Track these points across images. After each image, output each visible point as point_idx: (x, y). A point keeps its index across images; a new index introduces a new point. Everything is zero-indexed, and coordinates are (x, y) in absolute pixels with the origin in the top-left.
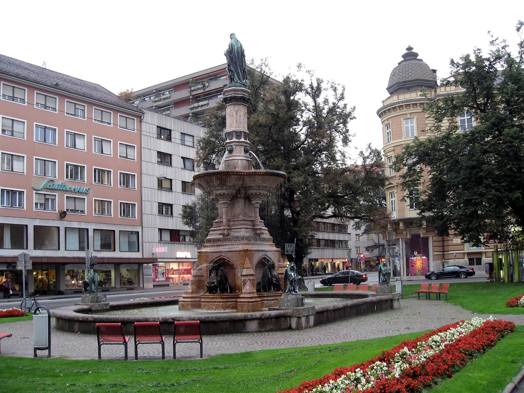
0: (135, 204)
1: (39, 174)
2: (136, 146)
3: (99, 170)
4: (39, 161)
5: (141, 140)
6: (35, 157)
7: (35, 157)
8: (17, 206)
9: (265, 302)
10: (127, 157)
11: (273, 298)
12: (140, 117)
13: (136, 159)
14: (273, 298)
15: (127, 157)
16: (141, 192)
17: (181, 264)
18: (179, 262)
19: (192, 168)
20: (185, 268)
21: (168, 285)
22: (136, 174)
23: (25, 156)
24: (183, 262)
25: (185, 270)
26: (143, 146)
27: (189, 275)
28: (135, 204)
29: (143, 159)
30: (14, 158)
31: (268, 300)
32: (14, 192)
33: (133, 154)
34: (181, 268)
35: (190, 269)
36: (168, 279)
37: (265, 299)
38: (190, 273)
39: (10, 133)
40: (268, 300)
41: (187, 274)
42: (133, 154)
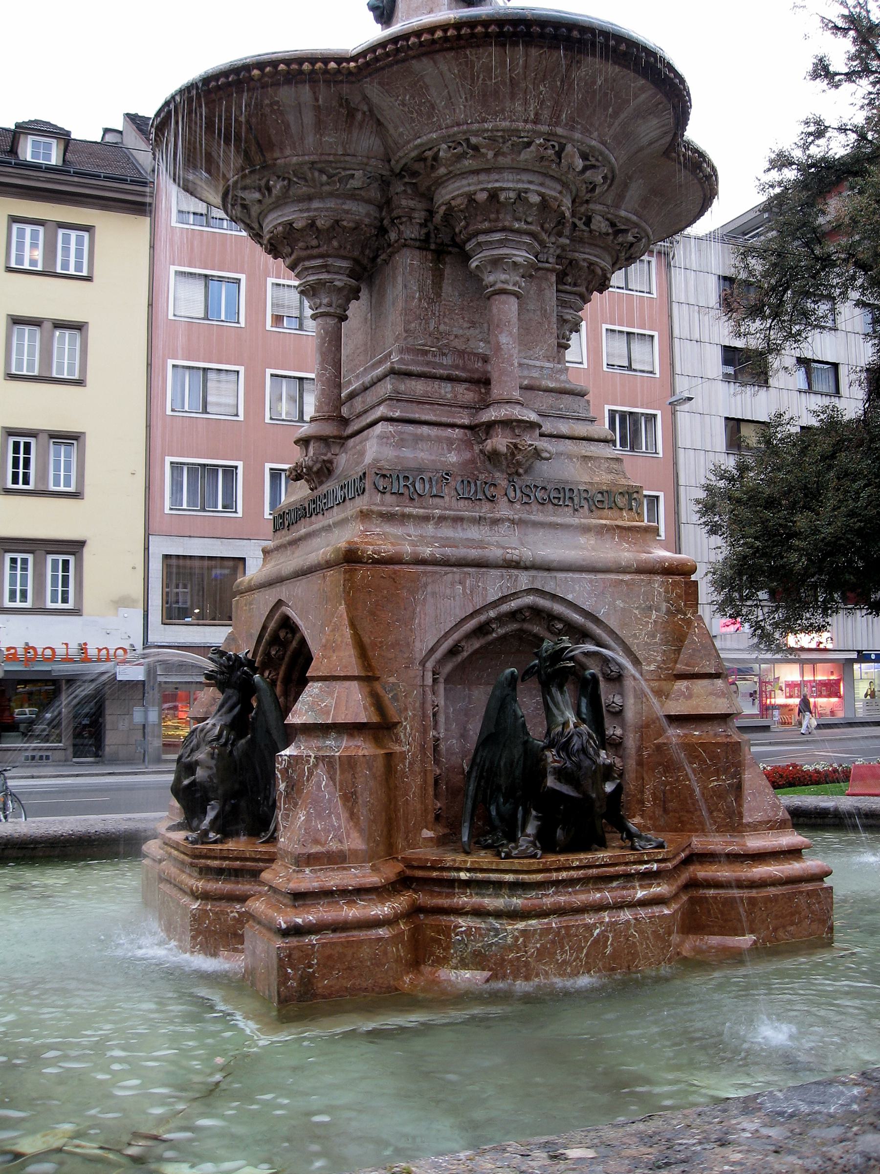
0: (657, 497)
1: (186, 408)
2: (655, 334)
3: (623, 415)
4: (284, 381)
5: (671, 316)
6: (269, 371)
7: (269, 371)
8: (220, 508)
9: (463, 923)
10: (630, 368)
11: (517, 902)
12: (667, 254)
13: (657, 371)
14: (517, 902)
15: (630, 368)
16: (675, 464)
17: (808, 668)
18: (802, 662)
19: (832, 389)
20: (820, 677)
21: (766, 728)
22: (658, 413)
23: (241, 369)
24: (813, 662)
25: (822, 684)
26: (676, 333)
27: (834, 700)
28: (657, 497)
29: (678, 370)
30: (211, 376)
31: (479, 913)
32: (213, 470)
33: (649, 357)
34: (808, 677)
35: (837, 682)
36: (766, 709)
37: (464, 900)
38: (836, 694)
39: (295, 324)
40: (479, 913)
41: (829, 696)
42: (649, 357)
